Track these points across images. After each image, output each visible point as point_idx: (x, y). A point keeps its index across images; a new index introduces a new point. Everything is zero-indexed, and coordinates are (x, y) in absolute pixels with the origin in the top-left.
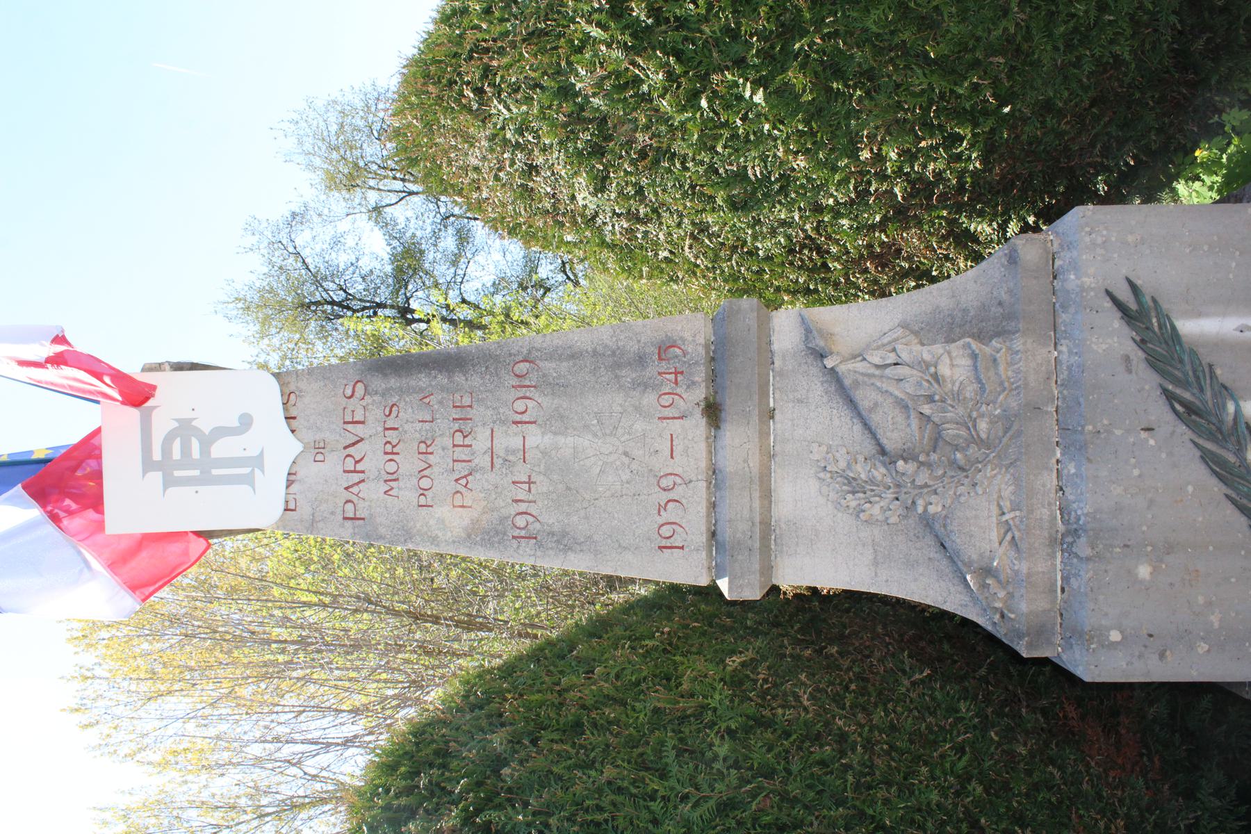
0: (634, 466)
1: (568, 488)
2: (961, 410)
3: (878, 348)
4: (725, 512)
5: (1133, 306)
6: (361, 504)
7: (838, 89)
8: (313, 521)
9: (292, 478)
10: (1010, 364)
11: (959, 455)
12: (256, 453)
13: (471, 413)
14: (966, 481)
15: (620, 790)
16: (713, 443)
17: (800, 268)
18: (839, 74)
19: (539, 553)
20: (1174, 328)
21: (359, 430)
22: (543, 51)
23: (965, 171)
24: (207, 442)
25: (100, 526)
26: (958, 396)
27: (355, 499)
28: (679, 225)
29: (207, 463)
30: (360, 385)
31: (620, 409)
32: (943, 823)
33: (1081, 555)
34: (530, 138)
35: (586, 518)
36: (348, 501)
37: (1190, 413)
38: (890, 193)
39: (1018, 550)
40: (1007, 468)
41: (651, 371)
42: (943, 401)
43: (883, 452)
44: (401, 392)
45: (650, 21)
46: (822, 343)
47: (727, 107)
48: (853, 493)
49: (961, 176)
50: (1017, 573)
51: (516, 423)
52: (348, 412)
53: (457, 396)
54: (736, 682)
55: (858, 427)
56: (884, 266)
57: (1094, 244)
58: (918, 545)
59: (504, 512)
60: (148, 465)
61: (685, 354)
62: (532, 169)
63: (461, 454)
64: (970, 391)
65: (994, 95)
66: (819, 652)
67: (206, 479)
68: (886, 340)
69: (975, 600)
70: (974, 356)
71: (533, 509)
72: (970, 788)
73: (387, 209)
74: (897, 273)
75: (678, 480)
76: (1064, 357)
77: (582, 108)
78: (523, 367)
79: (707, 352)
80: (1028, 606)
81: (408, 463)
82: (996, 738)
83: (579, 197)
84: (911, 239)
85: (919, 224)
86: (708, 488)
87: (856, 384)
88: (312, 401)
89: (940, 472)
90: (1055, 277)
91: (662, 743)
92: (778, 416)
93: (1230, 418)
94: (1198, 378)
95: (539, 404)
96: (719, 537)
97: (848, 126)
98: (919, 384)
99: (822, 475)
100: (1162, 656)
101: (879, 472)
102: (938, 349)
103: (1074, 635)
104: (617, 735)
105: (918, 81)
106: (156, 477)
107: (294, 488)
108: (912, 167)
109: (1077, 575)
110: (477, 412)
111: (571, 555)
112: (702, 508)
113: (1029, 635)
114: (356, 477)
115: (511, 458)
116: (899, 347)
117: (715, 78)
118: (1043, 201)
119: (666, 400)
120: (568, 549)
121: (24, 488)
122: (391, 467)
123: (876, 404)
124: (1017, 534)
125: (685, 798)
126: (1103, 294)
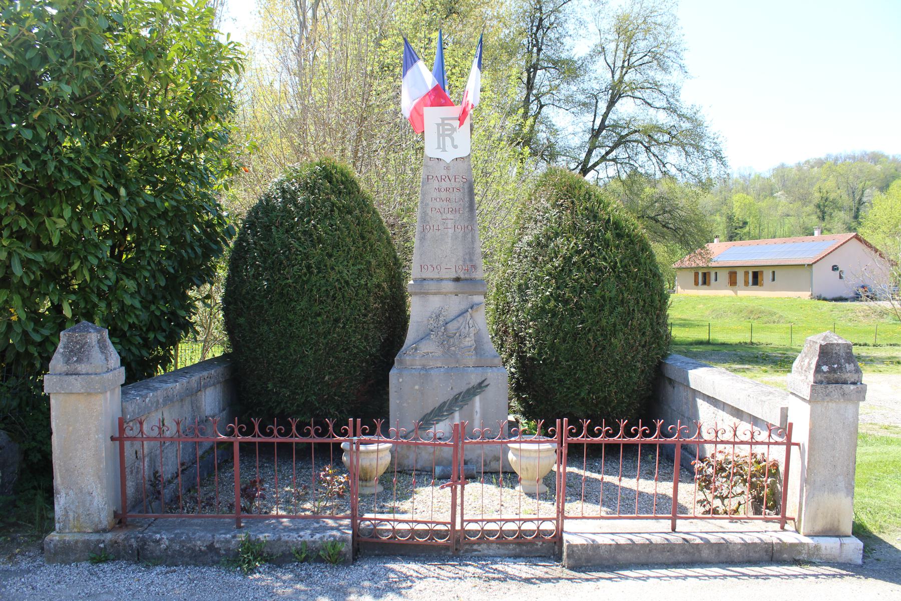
4: (431, 282)
13: (457, 213)
15: (348, 252)
16: (450, 279)
22: (570, 228)
25: (426, 106)
26: (460, 342)
29: (444, 136)
37: (456, 399)
43: (446, 324)
44: (464, 193)
47: (546, 284)
49: (526, 352)
54: (379, 286)
55: (453, 317)
60: (443, 119)
63: (446, 210)
67: (439, 135)
71: (431, 231)
73: (602, 57)
77: (551, 240)
78: (470, 228)
81: (444, 195)
84: (510, 339)
85: (514, 341)
91: (362, 264)
102: (473, 338)
106: (440, 122)
110: (458, 215)
112: (432, 277)
114: (440, 179)
119: (460, 267)
120: (421, 240)
122: (442, 190)
125: (348, 271)
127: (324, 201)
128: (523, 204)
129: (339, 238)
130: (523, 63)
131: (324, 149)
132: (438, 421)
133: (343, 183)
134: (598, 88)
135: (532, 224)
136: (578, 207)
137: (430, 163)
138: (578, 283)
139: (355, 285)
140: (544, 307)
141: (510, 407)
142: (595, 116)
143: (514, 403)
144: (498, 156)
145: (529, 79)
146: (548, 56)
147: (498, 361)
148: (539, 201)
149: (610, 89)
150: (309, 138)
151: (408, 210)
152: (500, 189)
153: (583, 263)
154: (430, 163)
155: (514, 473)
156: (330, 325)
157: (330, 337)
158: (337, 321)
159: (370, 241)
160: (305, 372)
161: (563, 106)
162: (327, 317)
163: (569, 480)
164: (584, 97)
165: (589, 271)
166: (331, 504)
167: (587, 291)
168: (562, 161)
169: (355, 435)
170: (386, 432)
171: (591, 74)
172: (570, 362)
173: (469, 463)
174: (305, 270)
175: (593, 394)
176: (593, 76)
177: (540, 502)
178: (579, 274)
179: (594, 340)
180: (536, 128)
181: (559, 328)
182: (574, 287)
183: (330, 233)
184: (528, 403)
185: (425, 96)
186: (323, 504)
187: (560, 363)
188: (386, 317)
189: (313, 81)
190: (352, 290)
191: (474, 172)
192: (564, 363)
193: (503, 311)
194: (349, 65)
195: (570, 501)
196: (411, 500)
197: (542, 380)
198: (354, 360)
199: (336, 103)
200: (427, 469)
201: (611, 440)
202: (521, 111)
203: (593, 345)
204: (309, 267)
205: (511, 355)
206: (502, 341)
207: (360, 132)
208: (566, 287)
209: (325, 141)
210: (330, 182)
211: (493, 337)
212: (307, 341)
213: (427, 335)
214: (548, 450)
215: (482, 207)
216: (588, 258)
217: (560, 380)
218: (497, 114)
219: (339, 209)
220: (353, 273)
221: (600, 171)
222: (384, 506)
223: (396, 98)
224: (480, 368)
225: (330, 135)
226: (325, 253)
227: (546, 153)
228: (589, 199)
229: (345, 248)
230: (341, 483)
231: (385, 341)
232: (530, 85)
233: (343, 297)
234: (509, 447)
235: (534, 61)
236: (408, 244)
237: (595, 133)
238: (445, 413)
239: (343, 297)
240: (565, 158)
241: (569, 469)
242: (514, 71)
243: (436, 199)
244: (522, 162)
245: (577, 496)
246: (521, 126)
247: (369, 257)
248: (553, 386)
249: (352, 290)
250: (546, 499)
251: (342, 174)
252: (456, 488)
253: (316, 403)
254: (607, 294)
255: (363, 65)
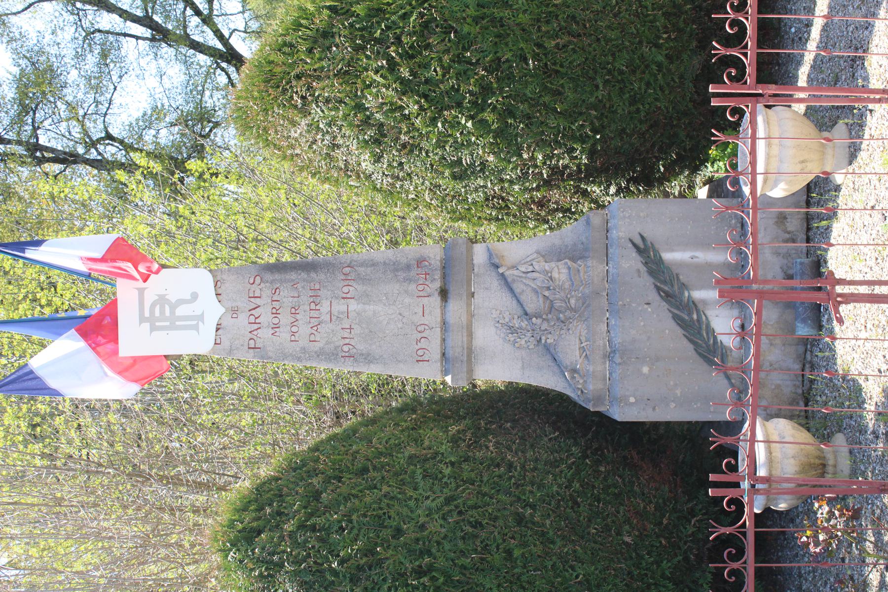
0: (404, 320)
1: (371, 331)
2: (562, 294)
3: (525, 263)
4: (449, 343)
5: (642, 246)
6: (258, 340)
7: (511, 123)
8: (231, 350)
9: (219, 327)
10: (585, 272)
11: (561, 315)
12: (199, 313)
13: (320, 293)
14: (565, 328)
15: (392, 498)
17: (492, 208)
18: (512, 114)
19: (355, 364)
20: (660, 257)
21: (258, 301)
22: (346, 83)
23: (580, 164)
24: (173, 307)
25: (116, 352)
26: (561, 288)
27: (255, 337)
28: (423, 184)
30: (258, 277)
31: (397, 292)
32: (559, 501)
33: (617, 362)
34: (335, 130)
35: (380, 346)
36: (251, 339)
37: (668, 297)
38: (542, 174)
39: (588, 360)
40: (584, 321)
41: (413, 273)
42: (554, 289)
43: (526, 314)
44: (282, 282)
45: (411, 78)
46: (497, 261)
47: (452, 127)
48: (512, 334)
49: (579, 166)
50: (588, 371)
51: (344, 298)
52: (251, 291)
53: (312, 284)
54: (455, 441)
55: (515, 302)
56: (542, 206)
57: (624, 217)
58: (543, 359)
59: (337, 344)
60: (142, 319)
61: (430, 265)
62: (335, 146)
63: (314, 314)
64: (567, 285)
65: (591, 130)
66: (500, 427)
67: (173, 327)
68: (528, 259)
69: (570, 385)
70: (569, 268)
72: (574, 485)
73: (13, 19)
74: (550, 210)
75: (427, 327)
76: (610, 270)
77: (369, 118)
78: (347, 270)
79: (441, 264)
80: (593, 387)
81: (285, 318)
82: (589, 463)
83: (363, 164)
84: (555, 195)
85: (558, 187)
86: (441, 331)
87: (514, 280)
88: (231, 285)
89: (553, 324)
90: (607, 231)
91: (414, 472)
92: (476, 296)
93: (686, 299)
94: (671, 280)
95: (356, 288)
96: (447, 356)
97: (516, 140)
98: (543, 281)
99: (497, 325)
100: (654, 409)
101: (524, 324)
102: (553, 264)
103: (615, 400)
104: (388, 471)
105: (552, 123)
106: (146, 326)
107: (220, 332)
108: (551, 162)
109: (615, 372)
111: (372, 366)
112: (438, 341)
113: (593, 400)
114: (256, 326)
115: (341, 316)
116: (534, 263)
117: (445, 113)
118: (629, 174)
119: (421, 288)
120: (370, 362)
121: (76, 330)
122: (276, 321)
123: (523, 291)
124: (588, 353)
126: (628, 241)
127: (295, 544)
128: (301, 169)
129: (365, 516)
130: (25, 172)
131: (193, 546)
132: (710, 331)
133: (261, 509)
134: (73, 29)
135: (338, 153)
136: (306, 67)
137: (226, 344)
138: (450, 67)
139: (453, 485)
140: (495, 131)
141: (682, 195)
142: (126, 35)
143: (675, 186)
144: (206, 219)
145: (55, 160)
146: (12, 124)
147: (596, 218)
148: (296, 140)
149: (74, 5)
150: (171, 575)
151: (310, 386)
152: (269, 214)
153: (412, 57)
154: (226, 344)
155: (809, 188)
156: (529, 533)
157: (551, 533)
158: (520, 520)
159: (370, 456)
160: (618, 581)
161: (109, 96)
162: (513, 538)
163: (824, 81)
164: (89, 56)
165: (428, 46)
166: (870, 532)
167: (465, 49)
168: (212, 100)
169: (737, 485)
170: (733, 427)
171: (45, 41)
172: (599, 81)
173: (790, 272)
174: (425, 580)
175: (659, 37)
176: (48, 38)
177: (866, 136)
178: (434, 64)
179: (557, 36)
180: (150, 147)
181: (534, 103)
182: (458, 75)
183: (355, 531)
184: (674, 162)
185: (98, 353)
186: (869, 547)
187: (600, 101)
188: (513, 428)
189: (61, 568)
190: (464, 491)
191: (236, 263)
192: (599, 94)
193: (501, 208)
194: (30, 500)
195: (866, 79)
196: (861, 381)
197: (630, 136)
198: (594, 487)
199: (105, 524)
200: (801, 349)
201: (750, 71)
202: (121, 175)
203: (566, 38)
204: (419, 572)
205: (585, 193)
206: (557, 210)
207: (162, 478)
208: (458, 90)
209: (176, 543)
210: (259, 533)
211: (550, 228)
212: (559, 576)
213: (548, 349)
214: (767, 122)
215: (303, 248)
216: (403, 48)
217: (633, 101)
218: (126, 221)
219: (311, 515)
220: (431, 489)
221: (233, 27)
222: (874, 432)
223: (98, 408)
224: (611, 251)
225: (167, 535)
226: (394, 542)
227: (198, 128)
228: (291, 46)
229: (383, 505)
230: (831, 514)
231: (558, 429)
232: (68, 159)
233: (475, 507)
234: (761, 195)
235: (20, 150)
236: (373, 388)
237: (160, 35)
238: (695, 317)
239: (475, 507)
240: (207, 93)
241: (802, 82)
242: (44, 187)
243: (293, 334)
244: (216, 175)
245: (856, 63)
246: (149, 174)
247: (401, 459)
248: (643, 114)
249: (464, 491)
250: (862, 126)
251: (245, 509)
252: (840, 295)
253: (676, 560)
254: (471, 12)
255: (31, 473)
